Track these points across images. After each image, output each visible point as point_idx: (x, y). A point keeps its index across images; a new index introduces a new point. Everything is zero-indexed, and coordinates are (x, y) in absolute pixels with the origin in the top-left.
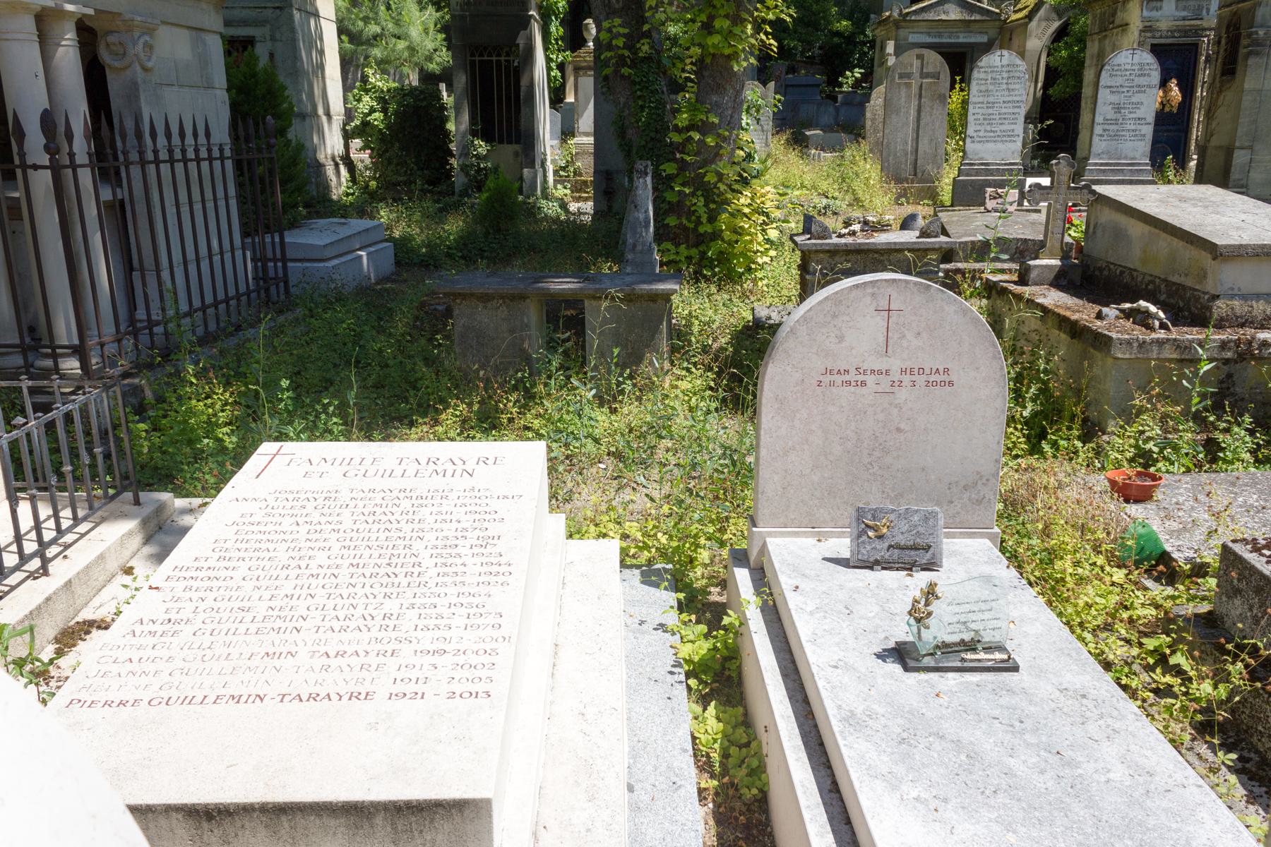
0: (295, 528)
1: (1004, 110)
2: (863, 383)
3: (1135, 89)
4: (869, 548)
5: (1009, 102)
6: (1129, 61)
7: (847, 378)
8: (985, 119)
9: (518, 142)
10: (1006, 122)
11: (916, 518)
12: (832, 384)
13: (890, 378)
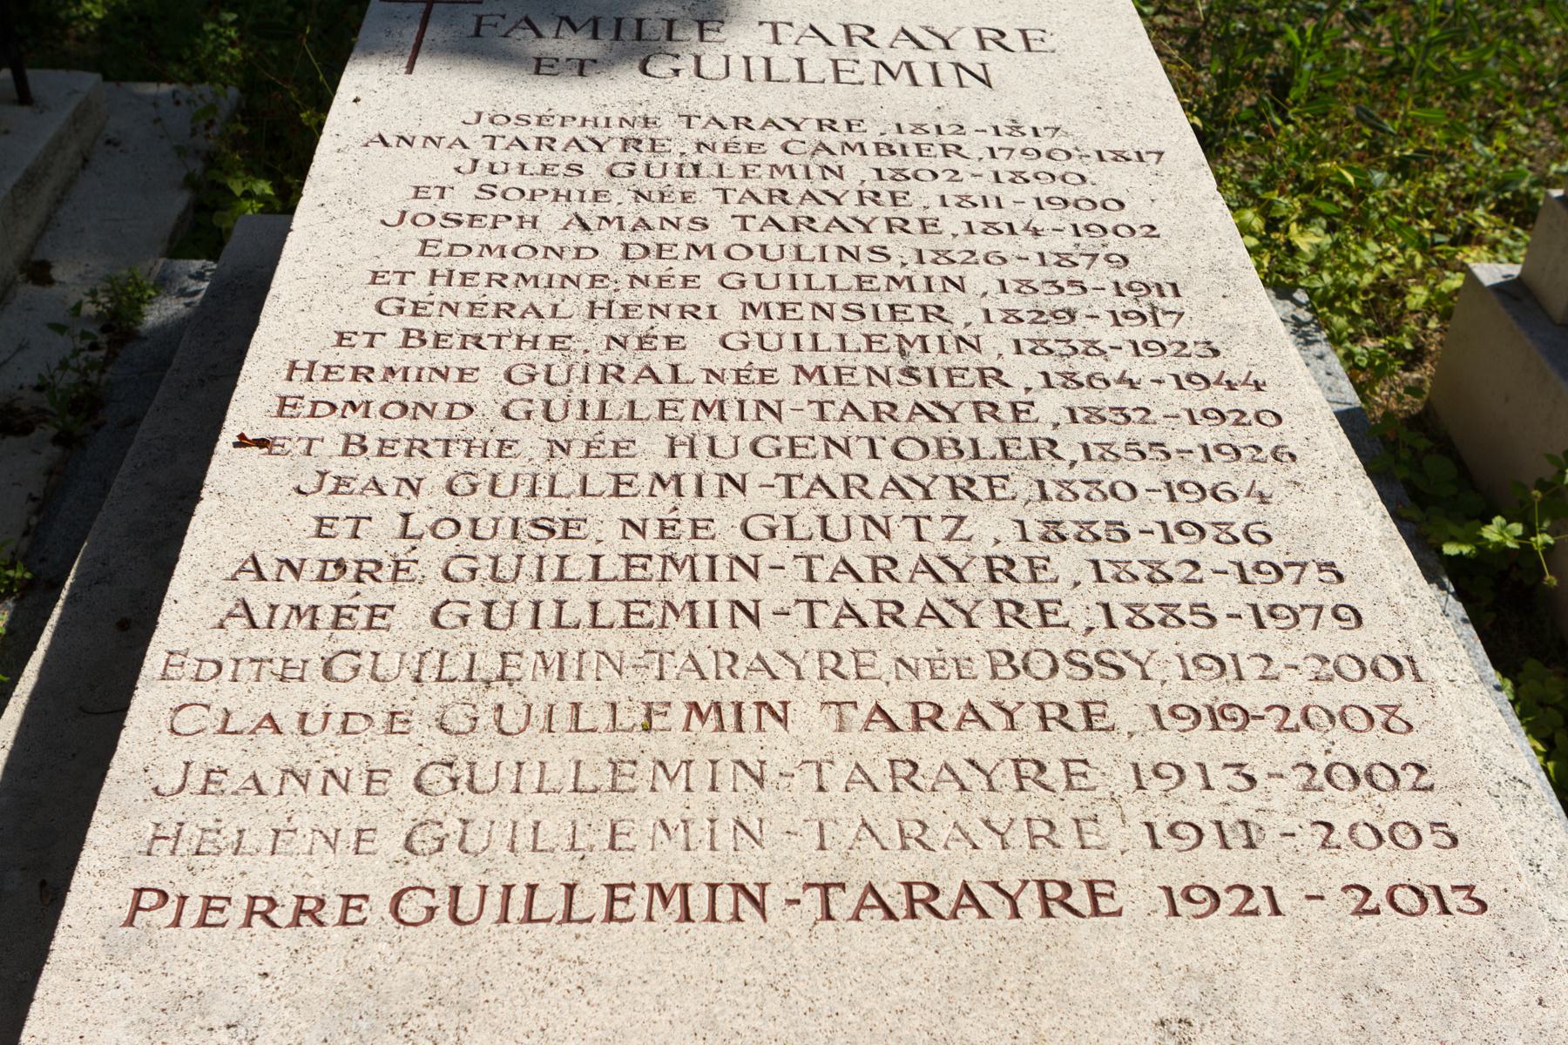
0: (576, 236)
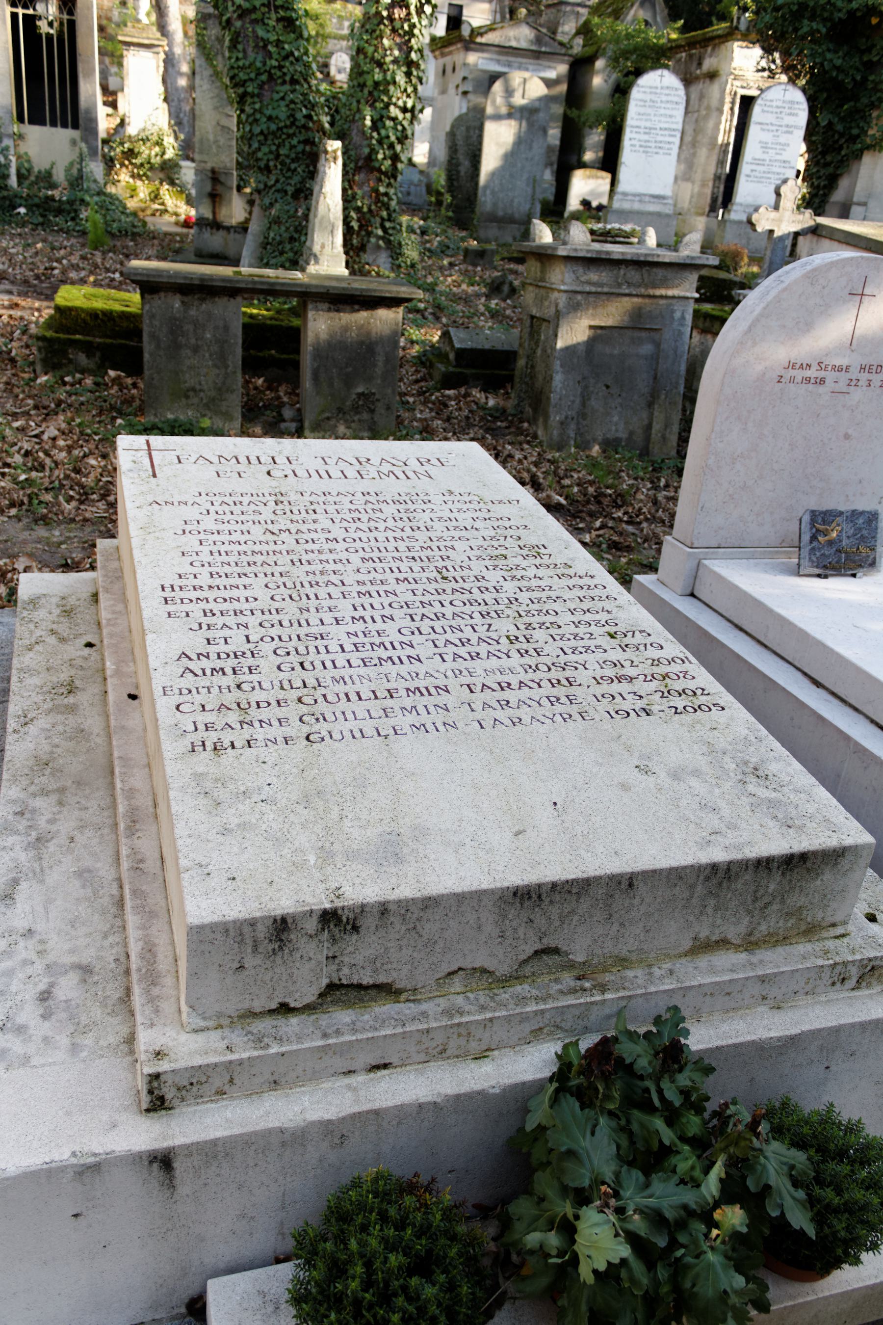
1: (659, 138)
2: (822, 381)
3: (785, 129)
4: (818, 554)
5: (666, 129)
6: (781, 97)
7: (808, 373)
8: (641, 146)
9: (75, 126)
10: (661, 151)
11: (861, 521)
12: (792, 380)
13: (848, 376)
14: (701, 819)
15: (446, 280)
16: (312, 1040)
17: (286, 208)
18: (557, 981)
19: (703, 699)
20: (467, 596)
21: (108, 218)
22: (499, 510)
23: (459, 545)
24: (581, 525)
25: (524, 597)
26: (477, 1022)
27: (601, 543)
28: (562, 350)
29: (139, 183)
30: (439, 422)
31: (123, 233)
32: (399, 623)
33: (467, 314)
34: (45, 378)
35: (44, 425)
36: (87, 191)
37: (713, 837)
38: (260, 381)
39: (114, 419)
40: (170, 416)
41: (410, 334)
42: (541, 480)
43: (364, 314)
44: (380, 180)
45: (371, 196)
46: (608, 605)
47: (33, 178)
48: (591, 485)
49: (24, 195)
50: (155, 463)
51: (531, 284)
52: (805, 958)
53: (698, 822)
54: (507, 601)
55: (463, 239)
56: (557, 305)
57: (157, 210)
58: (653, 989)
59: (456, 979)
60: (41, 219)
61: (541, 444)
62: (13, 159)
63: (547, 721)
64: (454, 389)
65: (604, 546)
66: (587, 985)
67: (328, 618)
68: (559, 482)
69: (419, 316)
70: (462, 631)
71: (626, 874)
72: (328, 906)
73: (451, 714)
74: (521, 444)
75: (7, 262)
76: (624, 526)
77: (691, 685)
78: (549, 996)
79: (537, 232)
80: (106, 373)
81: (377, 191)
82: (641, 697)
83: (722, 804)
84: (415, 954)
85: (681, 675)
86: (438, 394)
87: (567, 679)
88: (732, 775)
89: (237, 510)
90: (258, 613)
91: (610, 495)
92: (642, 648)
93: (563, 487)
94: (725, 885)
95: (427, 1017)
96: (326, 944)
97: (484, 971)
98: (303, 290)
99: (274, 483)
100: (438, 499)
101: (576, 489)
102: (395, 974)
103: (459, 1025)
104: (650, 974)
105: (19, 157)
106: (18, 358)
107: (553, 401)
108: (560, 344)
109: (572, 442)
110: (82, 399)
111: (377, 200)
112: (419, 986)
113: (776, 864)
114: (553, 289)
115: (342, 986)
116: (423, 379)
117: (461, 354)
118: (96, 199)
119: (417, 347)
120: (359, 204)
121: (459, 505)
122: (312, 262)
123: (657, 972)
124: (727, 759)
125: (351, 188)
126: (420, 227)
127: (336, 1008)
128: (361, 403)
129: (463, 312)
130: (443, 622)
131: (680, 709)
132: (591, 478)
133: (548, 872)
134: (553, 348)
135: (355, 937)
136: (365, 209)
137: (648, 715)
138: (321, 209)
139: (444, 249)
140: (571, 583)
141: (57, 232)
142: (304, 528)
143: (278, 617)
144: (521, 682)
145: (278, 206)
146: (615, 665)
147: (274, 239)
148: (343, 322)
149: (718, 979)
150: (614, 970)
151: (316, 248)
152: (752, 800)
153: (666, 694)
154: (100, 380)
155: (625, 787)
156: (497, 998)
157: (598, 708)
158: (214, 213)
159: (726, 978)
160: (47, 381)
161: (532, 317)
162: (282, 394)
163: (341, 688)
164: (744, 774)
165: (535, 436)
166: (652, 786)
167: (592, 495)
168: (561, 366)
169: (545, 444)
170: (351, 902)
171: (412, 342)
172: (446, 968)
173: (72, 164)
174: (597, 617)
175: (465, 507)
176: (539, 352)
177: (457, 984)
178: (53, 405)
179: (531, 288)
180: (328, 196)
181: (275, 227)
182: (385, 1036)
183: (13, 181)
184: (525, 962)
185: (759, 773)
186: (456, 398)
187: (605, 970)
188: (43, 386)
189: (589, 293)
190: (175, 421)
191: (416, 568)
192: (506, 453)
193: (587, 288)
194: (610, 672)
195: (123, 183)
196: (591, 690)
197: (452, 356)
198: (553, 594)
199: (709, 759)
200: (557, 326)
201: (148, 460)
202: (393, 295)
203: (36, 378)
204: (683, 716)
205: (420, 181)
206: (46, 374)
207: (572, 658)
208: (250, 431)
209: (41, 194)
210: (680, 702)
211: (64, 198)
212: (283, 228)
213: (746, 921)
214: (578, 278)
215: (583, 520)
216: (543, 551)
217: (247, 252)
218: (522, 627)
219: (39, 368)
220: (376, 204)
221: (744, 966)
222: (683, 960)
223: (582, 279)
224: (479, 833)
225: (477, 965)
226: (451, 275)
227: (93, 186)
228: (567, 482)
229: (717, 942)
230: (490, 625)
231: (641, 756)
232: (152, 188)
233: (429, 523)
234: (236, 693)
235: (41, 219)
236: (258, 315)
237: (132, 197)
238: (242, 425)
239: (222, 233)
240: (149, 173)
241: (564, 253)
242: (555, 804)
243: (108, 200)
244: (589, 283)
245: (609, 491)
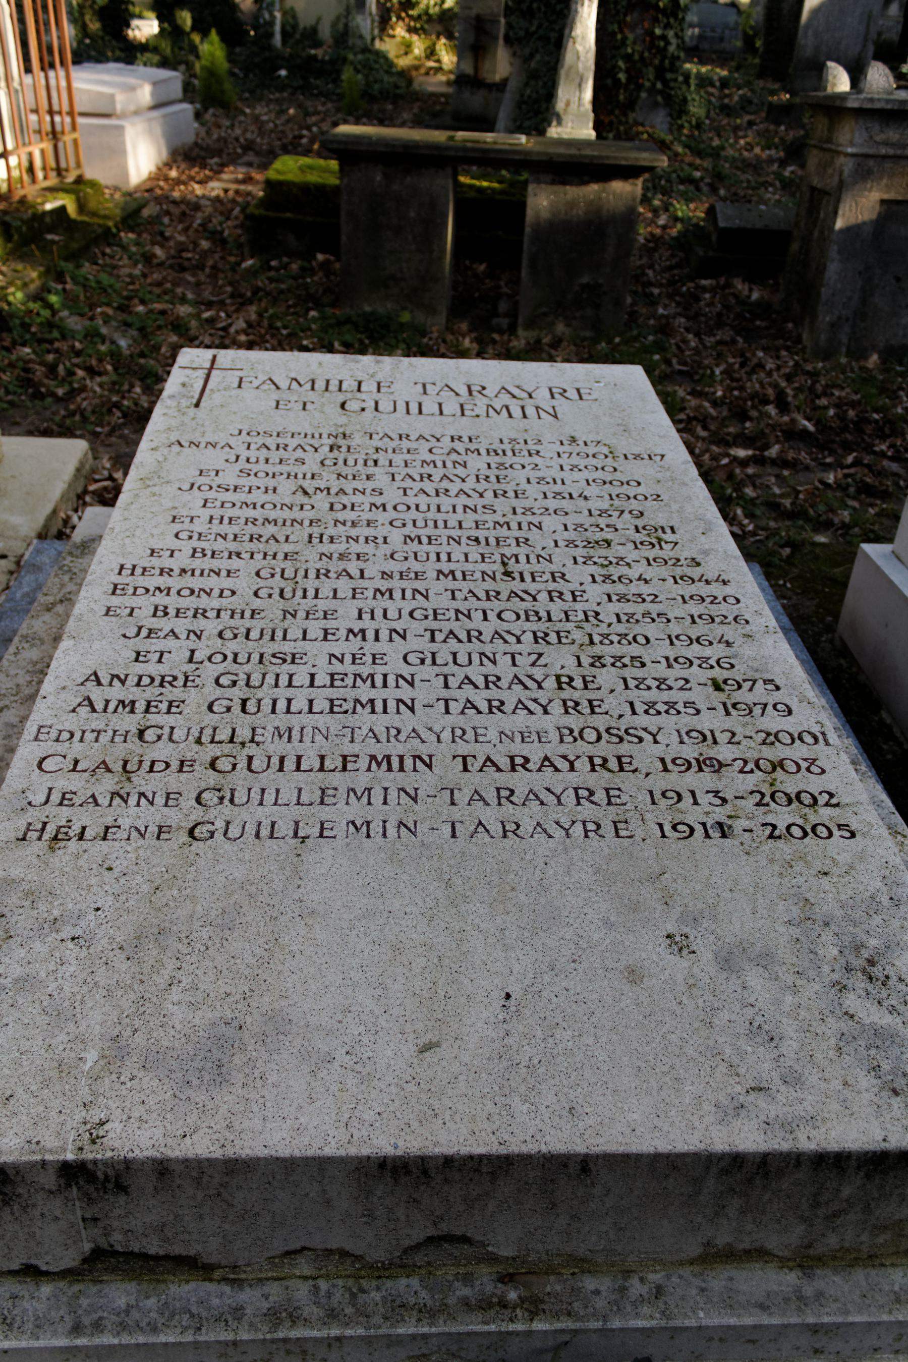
14: (742, 1055)
15: (736, 142)
16: (55, 1334)
17: (547, 58)
18: (467, 1279)
19: (825, 814)
20: (528, 605)
21: (371, 78)
22: (631, 470)
23: (551, 523)
24: (828, 460)
25: (608, 611)
26: (316, 1340)
27: (848, 485)
28: (842, 231)
29: (415, 38)
30: (683, 320)
31: (386, 95)
32: (413, 643)
33: (753, 184)
34: (250, 262)
35: (235, 316)
36: (352, 48)
37: (753, 1096)
38: (482, 267)
39: (308, 310)
40: (367, 309)
41: (676, 210)
42: (790, 399)
43: (595, 187)
44: (656, 20)
45: (644, 41)
46: (730, 632)
47: (298, 36)
48: (853, 408)
49: (287, 55)
50: (209, 387)
51: (815, 146)
52: (898, 1300)
53: (736, 1061)
54: (581, 616)
55: (773, 93)
56: (841, 173)
57: (431, 68)
58: (616, 1324)
59: (301, 1260)
60: (301, 82)
61: (803, 350)
62: (278, 15)
63: (559, 833)
64: (711, 278)
65: (852, 490)
66: (513, 1296)
67: (315, 629)
68: (813, 401)
69: (692, 188)
70: (494, 662)
71: (577, 1155)
72: (70, 1156)
73: (417, 808)
74: (778, 349)
75: (256, 131)
76: (885, 463)
77: (814, 784)
78: (444, 1308)
79: (830, 78)
80: (315, 258)
81: (652, 34)
82: (724, 801)
83: (789, 1028)
84: (227, 1226)
85: (804, 765)
86: (691, 285)
87: (619, 758)
88: (826, 969)
89: (275, 456)
90: (225, 615)
91: (876, 421)
92: (757, 710)
93: (816, 408)
94: (758, 1181)
95: (239, 1319)
96: (77, 1203)
97: (344, 1254)
98: (522, 157)
99: (343, 420)
100: (549, 450)
101: (831, 412)
102: (199, 1248)
103: (285, 1340)
104: (623, 1290)
105: (285, 13)
106: (230, 239)
107: (824, 297)
108: (839, 224)
109: (844, 350)
110: (283, 286)
111: (652, 45)
112: (241, 1263)
113: (853, 1163)
114: (839, 153)
115: (115, 1253)
116: (678, 266)
117: (725, 233)
118: (360, 57)
119: (679, 226)
120: (629, 50)
121: (575, 460)
122: (554, 123)
123: (636, 1288)
124: (827, 937)
125: (621, 31)
126: (721, 79)
127: (113, 1277)
128: (584, 296)
129: (748, 181)
130: (476, 646)
131: (781, 829)
132: (856, 397)
133: (443, 1137)
134: (831, 228)
135: (122, 1199)
136: (636, 57)
137: (724, 836)
138: (569, 58)
139: (745, 105)
140: (693, 589)
141: (316, 96)
142: (349, 487)
143: (248, 623)
144: (546, 758)
145: (538, 57)
146: (705, 738)
147: (529, 97)
148: (569, 197)
149: (733, 1321)
150: (566, 1272)
151: (560, 106)
152: (845, 1025)
153: (767, 799)
154: (306, 264)
155: (634, 975)
156: (362, 1298)
157: (648, 816)
158: (476, 68)
159: (748, 1321)
160: (252, 266)
161: (813, 189)
162: (502, 283)
163: (278, 747)
164: (848, 969)
165: (799, 340)
166: (680, 978)
167: (852, 421)
168: (839, 252)
169: (808, 351)
170: (109, 1154)
171: (676, 219)
172: (279, 1246)
173: (338, 18)
174: (707, 652)
175: (582, 463)
176: (816, 234)
177: (304, 1267)
178: (249, 294)
179: (815, 152)
180: (579, 40)
181: (533, 82)
182: (166, 1344)
183: (277, 39)
184: (417, 1247)
185: (877, 971)
186: (713, 290)
187: (551, 1271)
188: (248, 270)
189: (885, 157)
190: (373, 313)
191: (474, 556)
192: (755, 361)
193: (883, 151)
194: (690, 752)
195: (398, 39)
196: (649, 783)
197: (714, 238)
198: (654, 609)
199: (795, 932)
200: (838, 201)
201: (201, 383)
202: (630, 163)
203: (243, 260)
204: (780, 844)
205: (737, 23)
206: (252, 257)
207: (643, 720)
208: (456, 327)
209: (304, 54)
210: (783, 816)
211: (327, 58)
212: (541, 83)
213: (800, 1229)
214: (871, 137)
215: (832, 452)
216: (669, 536)
217: (503, 116)
218: (586, 661)
219: (246, 250)
220: (649, 50)
221: (787, 1300)
222: (686, 1271)
223: (878, 138)
224: (365, 1040)
225: (334, 1246)
226: (745, 137)
227: (359, 42)
228: (824, 402)
229: (747, 1252)
230: (540, 655)
231: (682, 919)
232: (428, 43)
233: (524, 485)
234: (134, 744)
235: (301, 82)
236: (488, 188)
237: (406, 54)
238: (448, 321)
239: (482, 92)
240: (426, 26)
241: (855, 105)
242: (508, 996)
243: (372, 57)
244: (886, 143)
245: (876, 416)
